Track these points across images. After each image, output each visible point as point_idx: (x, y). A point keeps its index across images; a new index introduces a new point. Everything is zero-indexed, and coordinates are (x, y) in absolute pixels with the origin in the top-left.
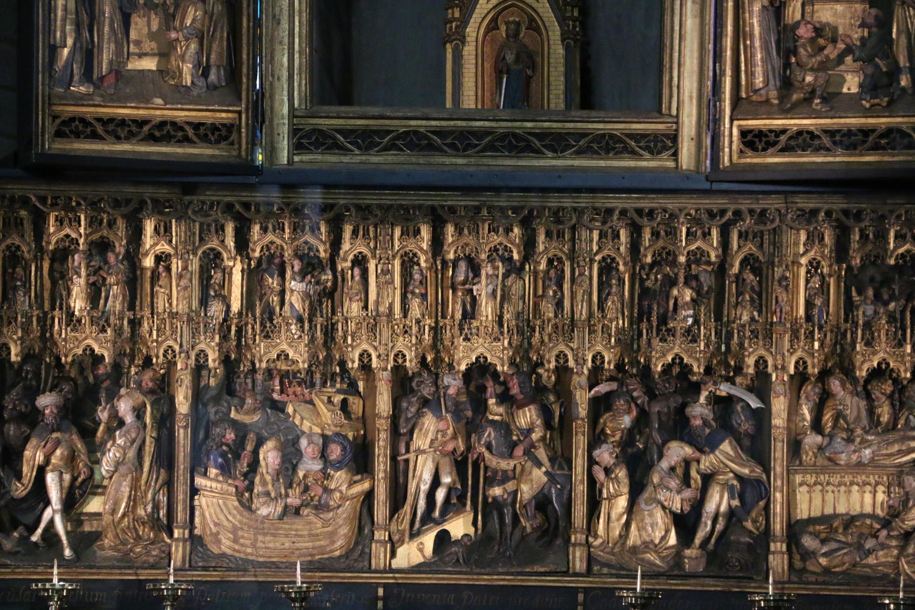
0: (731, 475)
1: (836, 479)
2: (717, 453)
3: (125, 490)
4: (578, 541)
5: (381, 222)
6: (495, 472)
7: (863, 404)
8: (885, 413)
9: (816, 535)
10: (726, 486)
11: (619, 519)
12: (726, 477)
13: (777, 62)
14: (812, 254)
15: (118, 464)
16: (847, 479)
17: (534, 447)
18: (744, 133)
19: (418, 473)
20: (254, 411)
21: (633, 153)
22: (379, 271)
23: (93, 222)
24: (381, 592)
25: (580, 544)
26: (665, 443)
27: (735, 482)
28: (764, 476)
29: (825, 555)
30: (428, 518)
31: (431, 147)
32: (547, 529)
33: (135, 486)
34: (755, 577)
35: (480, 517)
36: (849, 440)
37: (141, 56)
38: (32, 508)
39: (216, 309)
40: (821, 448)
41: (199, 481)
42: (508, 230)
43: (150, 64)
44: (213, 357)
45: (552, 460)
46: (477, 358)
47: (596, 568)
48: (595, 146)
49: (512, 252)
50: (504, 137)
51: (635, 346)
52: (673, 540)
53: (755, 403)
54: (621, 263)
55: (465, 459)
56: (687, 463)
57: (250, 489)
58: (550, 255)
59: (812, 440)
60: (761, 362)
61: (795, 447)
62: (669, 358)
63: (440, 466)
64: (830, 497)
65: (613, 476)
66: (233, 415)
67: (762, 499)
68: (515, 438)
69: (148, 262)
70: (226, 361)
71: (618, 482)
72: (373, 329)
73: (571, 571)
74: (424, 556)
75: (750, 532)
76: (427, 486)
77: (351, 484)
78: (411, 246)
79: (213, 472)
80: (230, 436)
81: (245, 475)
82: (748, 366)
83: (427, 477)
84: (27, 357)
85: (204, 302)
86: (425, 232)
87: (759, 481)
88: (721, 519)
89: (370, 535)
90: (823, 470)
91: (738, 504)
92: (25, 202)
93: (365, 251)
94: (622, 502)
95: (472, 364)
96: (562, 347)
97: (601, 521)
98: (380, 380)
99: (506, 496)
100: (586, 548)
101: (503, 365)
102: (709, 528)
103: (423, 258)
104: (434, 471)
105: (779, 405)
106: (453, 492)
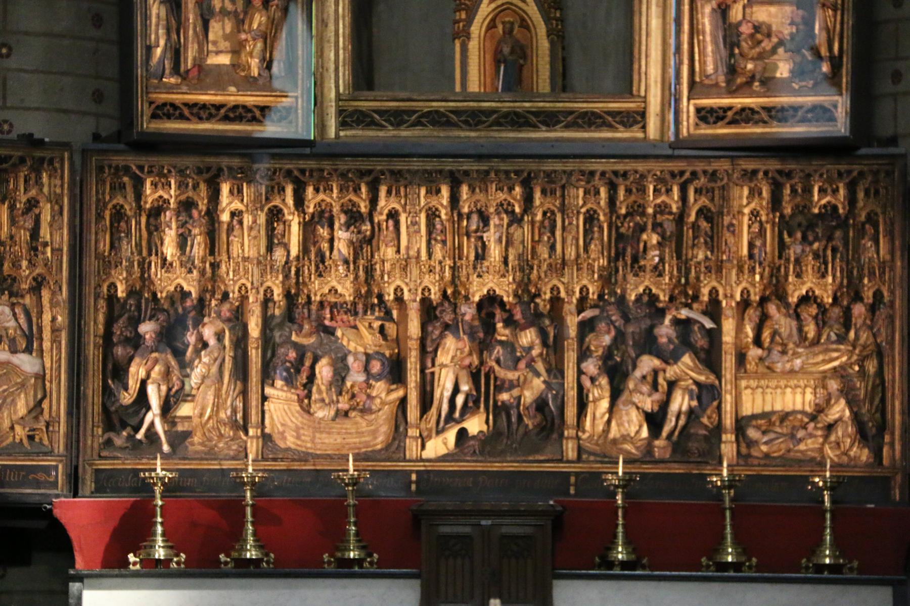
1: (793, 383)
2: (679, 364)
3: (210, 398)
5: (410, 183)
6: (503, 381)
7: (794, 323)
8: (811, 330)
9: (758, 427)
11: (602, 417)
13: (724, 53)
14: (753, 205)
15: (204, 378)
16: (783, 383)
18: (698, 110)
19: (442, 383)
20: (310, 335)
21: (610, 127)
23: (181, 185)
24: (414, 477)
25: (572, 438)
27: (694, 387)
29: (766, 443)
31: (449, 124)
33: (218, 395)
36: (784, 353)
37: (218, 53)
38: (137, 413)
39: (279, 255)
40: (761, 359)
41: (268, 391)
42: (511, 189)
43: (224, 60)
45: (548, 371)
48: (580, 121)
50: (506, 115)
51: (613, 280)
52: (645, 433)
53: (709, 324)
56: (655, 372)
57: (309, 396)
58: (545, 208)
59: (754, 353)
60: (714, 292)
61: (741, 359)
62: (641, 290)
64: (768, 398)
65: (597, 383)
68: (518, 354)
69: (225, 217)
70: (288, 295)
72: (404, 269)
74: (448, 449)
75: (706, 426)
77: (389, 392)
79: (279, 383)
80: (292, 355)
81: (305, 386)
83: (449, 386)
84: (131, 293)
85: (270, 248)
86: (445, 192)
87: (712, 386)
90: (763, 376)
93: (398, 207)
94: (605, 404)
99: (512, 400)
102: (673, 423)
105: (728, 326)
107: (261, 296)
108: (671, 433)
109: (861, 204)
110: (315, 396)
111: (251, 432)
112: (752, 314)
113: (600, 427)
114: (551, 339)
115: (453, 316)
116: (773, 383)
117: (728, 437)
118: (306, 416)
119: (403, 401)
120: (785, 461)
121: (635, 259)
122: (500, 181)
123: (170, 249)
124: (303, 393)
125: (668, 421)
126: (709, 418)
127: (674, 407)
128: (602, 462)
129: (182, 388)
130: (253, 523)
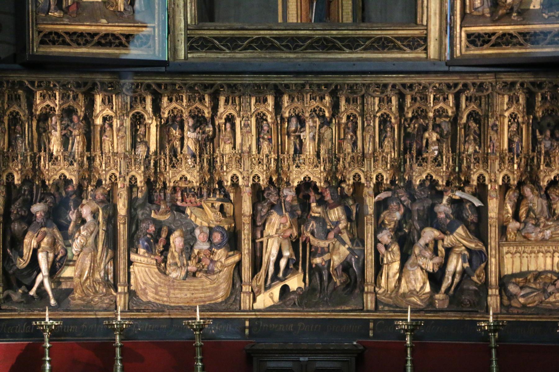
0: (463, 248)
1: (544, 249)
2: (455, 234)
4: (369, 291)
5: (243, 94)
6: (317, 248)
7: (545, 202)
9: (517, 284)
10: (460, 254)
11: (394, 276)
12: (460, 249)
14: (512, 110)
15: (83, 247)
16: (536, 249)
18: (469, 35)
19: (269, 250)
20: (166, 213)
21: (400, 49)
22: (242, 125)
23: (64, 97)
24: (247, 323)
25: (371, 293)
26: (422, 228)
27: (466, 252)
28: (484, 249)
29: (523, 296)
30: (275, 277)
31: (273, 48)
34: (479, 311)
35: (307, 277)
36: (537, 225)
38: (30, 275)
39: (141, 150)
41: (133, 257)
42: (322, 98)
44: (140, 180)
46: (304, 178)
47: (380, 307)
49: (324, 112)
50: (318, 40)
51: (402, 169)
52: (428, 289)
54: (393, 118)
55: (298, 241)
56: (436, 241)
57: (165, 261)
59: (513, 225)
60: (481, 178)
61: (503, 230)
62: (424, 176)
63: (283, 245)
64: (525, 260)
65: (390, 250)
66: (153, 215)
67: (483, 262)
68: (328, 227)
69: (99, 121)
70: (148, 182)
71: (394, 254)
72: (239, 161)
73: (365, 309)
74: (273, 301)
75: (476, 283)
77: (228, 257)
78: (262, 109)
79: (142, 251)
80: (152, 228)
82: (473, 181)
83: (275, 252)
84: (25, 181)
85: (134, 146)
86: (271, 101)
87: (481, 252)
88: (457, 275)
89: (240, 288)
90: (520, 244)
91: (468, 266)
92: (21, 84)
94: (396, 266)
96: (357, 171)
97: (383, 277)
98: (244, 193)
99: (324, 263)
102: (450, 281)
103: (269, 117)
104: (278, 248)
105: (493, 204)
106: (291, 261)
107: (127, 183)
108: (449, 289)
109: (463, 105)
110: (170, 261)
111: (120, 289)
112: (512, 195)
113: (393, 284)
114: (354, 215)
115: (277, 198)
116: (528, 249)
117: (493, 291)
118: (162, 276)
119: (239, 265)
120: (538, 310)
121: (419, 153)
122: (313, 92)
123: (55, 147)
124: (160, 259)
125: (446, 279)
126: (478, 276)
127: (451, 268)
128: (395, 312)
129: (66, 255)
130: (121, 361)
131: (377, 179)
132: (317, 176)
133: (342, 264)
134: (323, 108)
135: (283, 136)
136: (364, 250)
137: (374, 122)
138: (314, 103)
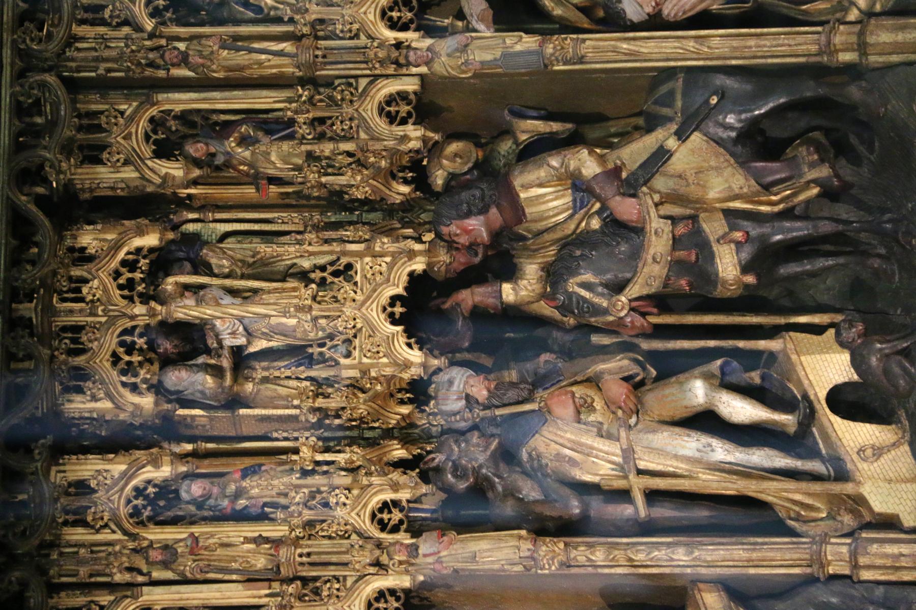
4: (854, 39)
5: (43, 571)
6: (677, 266)
17: (617, 170)
19: (681, 467)
22: (169, 575)
25: (861, 34)
32: (827, 132)
35: (803, 319)
42: (82, 257)
45: (652, 124)
46: (394, 322)
49: (139, 250)
55: (653, 357)
58: (147, 150)
63: (667, 414)
68: (595, 224)
74: (894, 445)
76: (716, 443)
89: (837, 586)
95: (409, 333)
96: (369, 110)
98: (439, 561)
99: (738, 235)
100: (873, 21)
101: (412, 255)
103: (149, 473)
104: (677, 430)
106: (732, 379)
114: (556, 126)
115: (475, 438)
122: (51, 289)
131: (405, 28)
132: (384, 267)
133: (743, 163)
134: (121, 255)
135: (246, 431)
136: (689, 69)
137: (179, 39)
138: (96, 283)
